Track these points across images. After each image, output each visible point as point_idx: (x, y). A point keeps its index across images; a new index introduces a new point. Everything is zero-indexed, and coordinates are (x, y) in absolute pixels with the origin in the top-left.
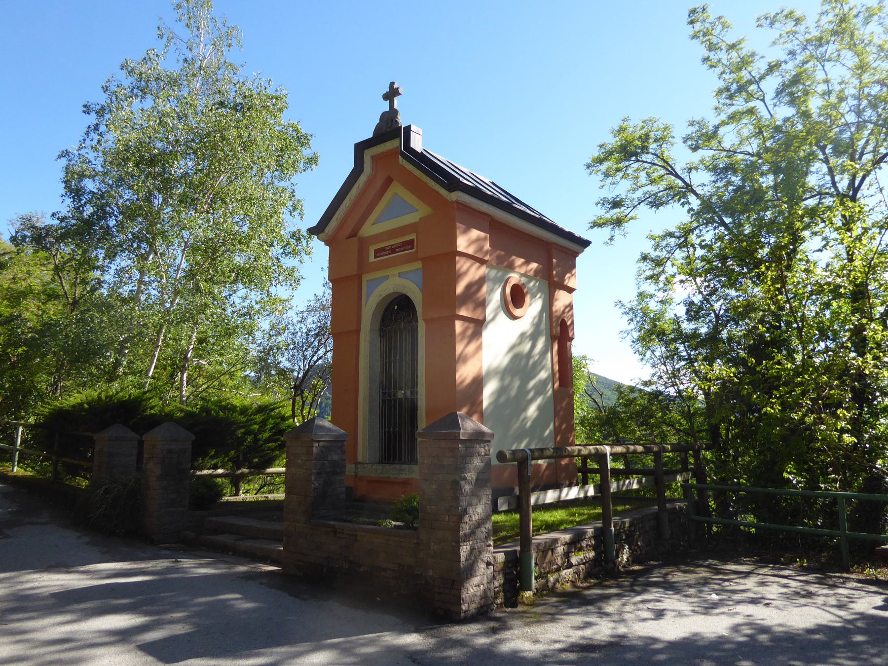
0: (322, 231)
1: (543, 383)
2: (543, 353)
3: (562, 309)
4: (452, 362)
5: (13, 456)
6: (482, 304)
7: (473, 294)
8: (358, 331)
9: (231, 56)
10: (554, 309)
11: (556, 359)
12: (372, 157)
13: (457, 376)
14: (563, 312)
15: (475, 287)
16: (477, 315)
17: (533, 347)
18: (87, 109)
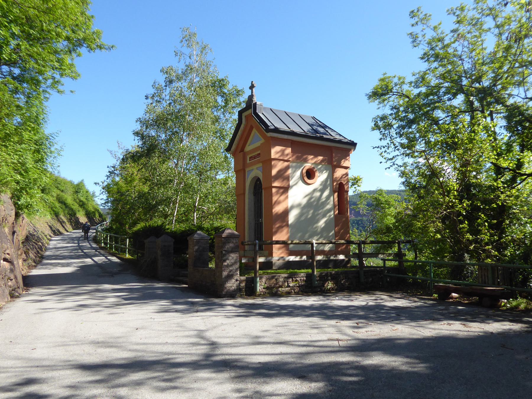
0: (230, 150)
1: (329, 211)
2: (328, 197)
3: (340, 176)
4: (271, 206)
5: (126, 251)
6: (288, 179)
7: (282, 175)
8: (244, 194)
9: (209, 57)
10: (335, 177)
11: (336, 199)
12: (245, 116)
13: (273, 211)
14: (341, 177)
15: (282, 173)
16: (284, 184)
17: (321, 195)
18: (147, 97)
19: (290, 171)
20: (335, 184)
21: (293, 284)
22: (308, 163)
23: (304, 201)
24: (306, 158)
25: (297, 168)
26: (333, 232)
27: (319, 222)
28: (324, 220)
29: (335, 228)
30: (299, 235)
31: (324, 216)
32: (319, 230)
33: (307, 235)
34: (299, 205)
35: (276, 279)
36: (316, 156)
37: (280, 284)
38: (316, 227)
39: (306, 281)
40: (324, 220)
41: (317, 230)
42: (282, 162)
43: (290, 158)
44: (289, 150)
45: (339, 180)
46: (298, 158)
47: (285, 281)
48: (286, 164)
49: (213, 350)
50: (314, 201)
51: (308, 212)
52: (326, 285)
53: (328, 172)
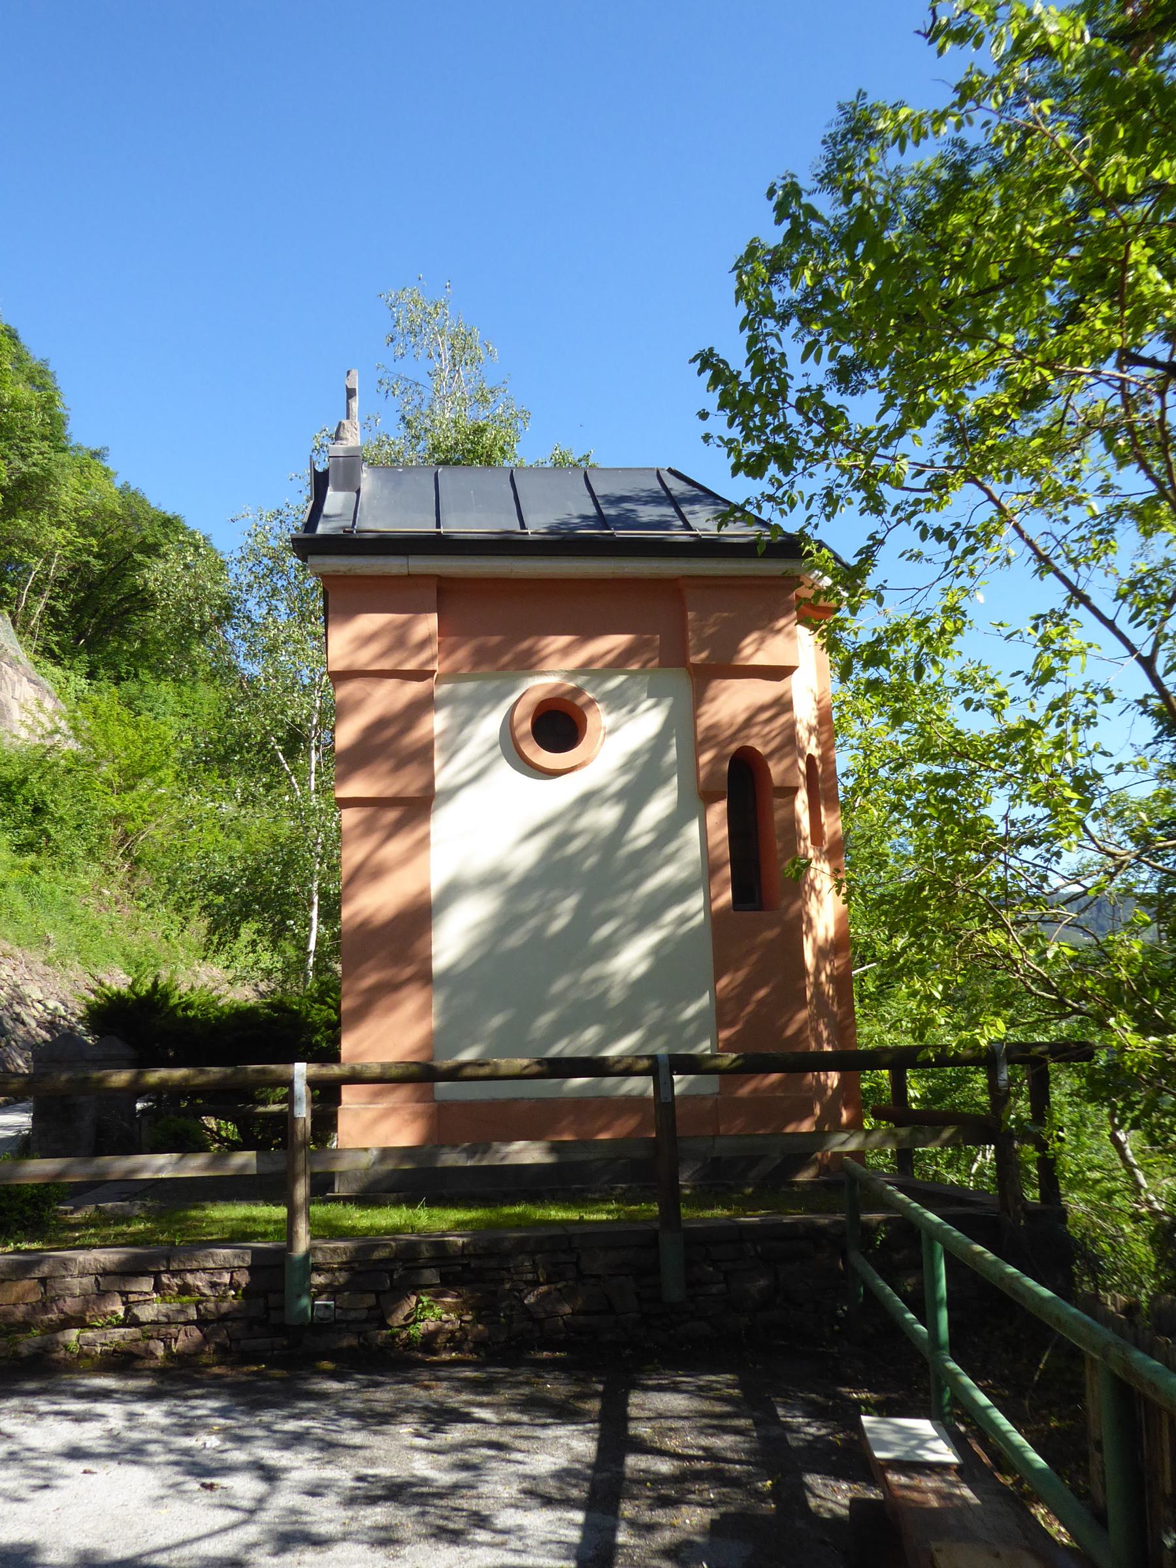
1: (677, 893)
2: (669, 829)
3: (741, 718)
6: (423, 754)
10: (704, 722)
14: (748, 723)
15: (390, 732)
16: (406, 783)
17: (627, 820)
19: (437, 722)
20: (705, 758)
21: (164, 1308)
22: (543, 673)
23: (526, 856)
24: (530, 653)
25: (478, 705)
26: (705, 1000)
27: (616, 954)
28: (649, 940)
29: (718, 977)
30: (496, 1021)
31: (647, 917)
32: (616, 995)
33: (545, 1019)
34: (489, 880)
35: (43, 1281)
36: (587, 633)
37: (70, 1305)
38: (596, 980)
39: (248, 1293)
40: (649, 940)
41: (606, 992)
42: (391, 683)
43: (432, 659)
44: (428, 624)
45: (733, 737)
46: (482, 657)
47: (102, 1294)
48: (414, 689)
49: (319, 1490)
50: (584, 851)
51: (548, 909)
52: (398, 1318)
53: (668, 702)
